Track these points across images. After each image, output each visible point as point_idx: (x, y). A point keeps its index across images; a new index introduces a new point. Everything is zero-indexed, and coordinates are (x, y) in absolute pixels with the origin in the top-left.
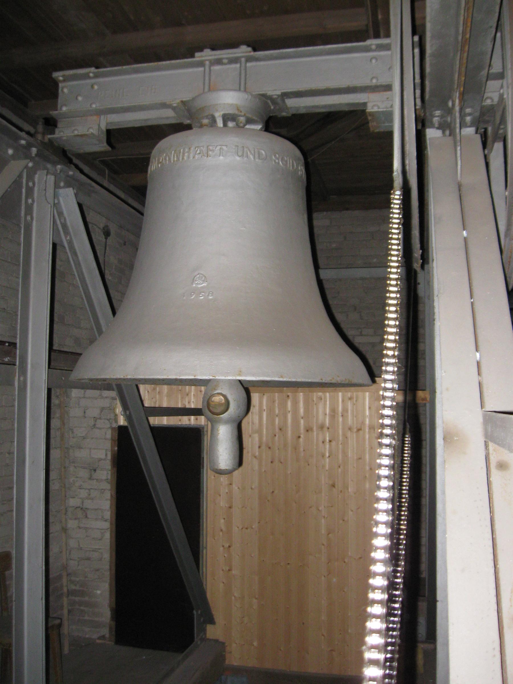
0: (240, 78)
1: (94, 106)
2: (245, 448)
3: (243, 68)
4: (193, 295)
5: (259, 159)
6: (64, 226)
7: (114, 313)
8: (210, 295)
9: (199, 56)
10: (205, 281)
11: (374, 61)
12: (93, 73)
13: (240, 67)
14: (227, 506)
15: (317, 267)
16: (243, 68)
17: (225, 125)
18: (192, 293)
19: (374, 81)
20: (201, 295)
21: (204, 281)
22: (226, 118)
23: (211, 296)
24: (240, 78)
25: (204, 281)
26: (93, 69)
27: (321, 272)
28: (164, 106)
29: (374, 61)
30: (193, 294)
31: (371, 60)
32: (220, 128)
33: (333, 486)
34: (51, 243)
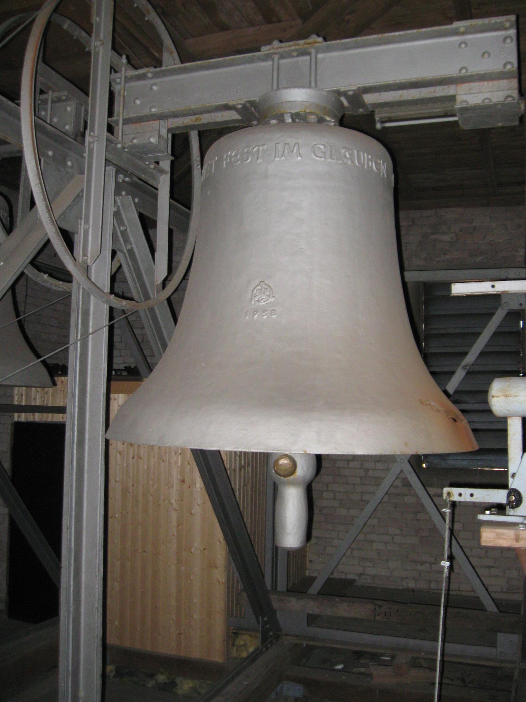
0: (310, 69)
1: (153, 110)
2: (417, 453)
3: (313, 60)
4: (256, 314)
5: (332, 158)
6: (124, 233)
7: (175, 320)
8: (273, 314)
9: (265, 50)
10: (271, 296)
11: (463, 46)
12: (152, 73)
13: (311, 59)
14: (179, 478)
15: (402, 269)
16: (313, 60)
17: (293, 121)
18: (254, 311)
19: (464, 71)
20: (264, 314)
21: (269, 296)
22: (295, 116)
23: (274, 315)
24: (310, 69)
25: (269, 296)
26: (152, 69)
27: (406, 274)
28: (227, 107)
29: (463, 46)
30: (255, 312)
31: (460, 45)
32: (288, 124)
33: (183, 481)
34: (111, 250)
